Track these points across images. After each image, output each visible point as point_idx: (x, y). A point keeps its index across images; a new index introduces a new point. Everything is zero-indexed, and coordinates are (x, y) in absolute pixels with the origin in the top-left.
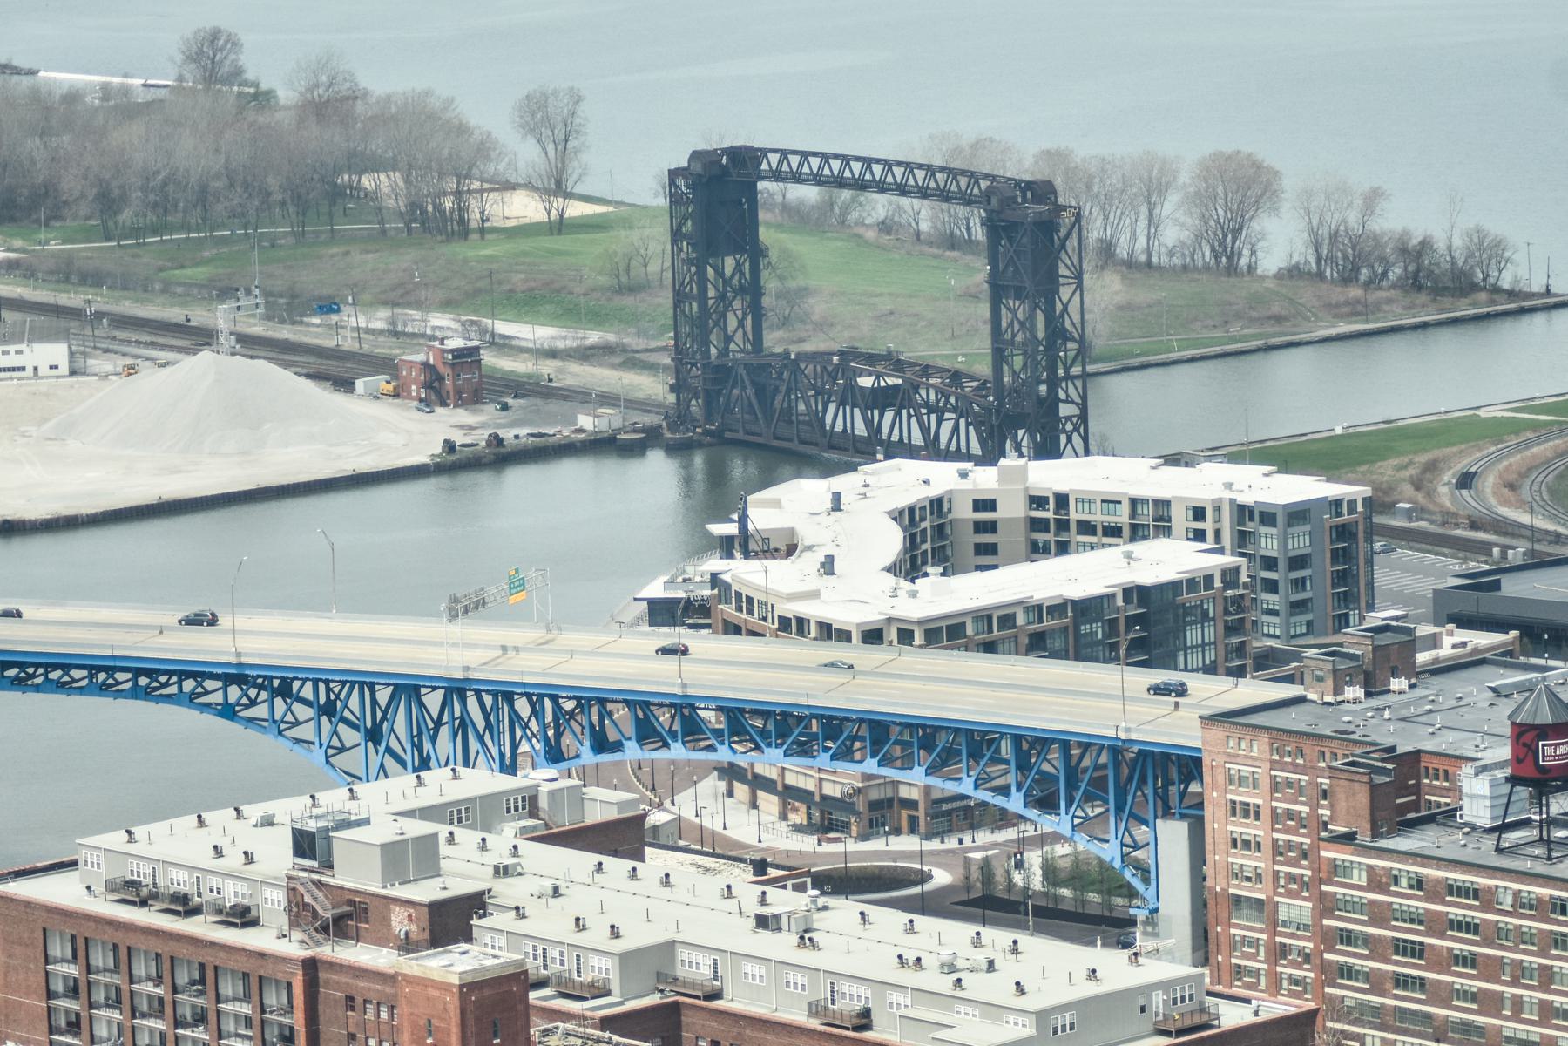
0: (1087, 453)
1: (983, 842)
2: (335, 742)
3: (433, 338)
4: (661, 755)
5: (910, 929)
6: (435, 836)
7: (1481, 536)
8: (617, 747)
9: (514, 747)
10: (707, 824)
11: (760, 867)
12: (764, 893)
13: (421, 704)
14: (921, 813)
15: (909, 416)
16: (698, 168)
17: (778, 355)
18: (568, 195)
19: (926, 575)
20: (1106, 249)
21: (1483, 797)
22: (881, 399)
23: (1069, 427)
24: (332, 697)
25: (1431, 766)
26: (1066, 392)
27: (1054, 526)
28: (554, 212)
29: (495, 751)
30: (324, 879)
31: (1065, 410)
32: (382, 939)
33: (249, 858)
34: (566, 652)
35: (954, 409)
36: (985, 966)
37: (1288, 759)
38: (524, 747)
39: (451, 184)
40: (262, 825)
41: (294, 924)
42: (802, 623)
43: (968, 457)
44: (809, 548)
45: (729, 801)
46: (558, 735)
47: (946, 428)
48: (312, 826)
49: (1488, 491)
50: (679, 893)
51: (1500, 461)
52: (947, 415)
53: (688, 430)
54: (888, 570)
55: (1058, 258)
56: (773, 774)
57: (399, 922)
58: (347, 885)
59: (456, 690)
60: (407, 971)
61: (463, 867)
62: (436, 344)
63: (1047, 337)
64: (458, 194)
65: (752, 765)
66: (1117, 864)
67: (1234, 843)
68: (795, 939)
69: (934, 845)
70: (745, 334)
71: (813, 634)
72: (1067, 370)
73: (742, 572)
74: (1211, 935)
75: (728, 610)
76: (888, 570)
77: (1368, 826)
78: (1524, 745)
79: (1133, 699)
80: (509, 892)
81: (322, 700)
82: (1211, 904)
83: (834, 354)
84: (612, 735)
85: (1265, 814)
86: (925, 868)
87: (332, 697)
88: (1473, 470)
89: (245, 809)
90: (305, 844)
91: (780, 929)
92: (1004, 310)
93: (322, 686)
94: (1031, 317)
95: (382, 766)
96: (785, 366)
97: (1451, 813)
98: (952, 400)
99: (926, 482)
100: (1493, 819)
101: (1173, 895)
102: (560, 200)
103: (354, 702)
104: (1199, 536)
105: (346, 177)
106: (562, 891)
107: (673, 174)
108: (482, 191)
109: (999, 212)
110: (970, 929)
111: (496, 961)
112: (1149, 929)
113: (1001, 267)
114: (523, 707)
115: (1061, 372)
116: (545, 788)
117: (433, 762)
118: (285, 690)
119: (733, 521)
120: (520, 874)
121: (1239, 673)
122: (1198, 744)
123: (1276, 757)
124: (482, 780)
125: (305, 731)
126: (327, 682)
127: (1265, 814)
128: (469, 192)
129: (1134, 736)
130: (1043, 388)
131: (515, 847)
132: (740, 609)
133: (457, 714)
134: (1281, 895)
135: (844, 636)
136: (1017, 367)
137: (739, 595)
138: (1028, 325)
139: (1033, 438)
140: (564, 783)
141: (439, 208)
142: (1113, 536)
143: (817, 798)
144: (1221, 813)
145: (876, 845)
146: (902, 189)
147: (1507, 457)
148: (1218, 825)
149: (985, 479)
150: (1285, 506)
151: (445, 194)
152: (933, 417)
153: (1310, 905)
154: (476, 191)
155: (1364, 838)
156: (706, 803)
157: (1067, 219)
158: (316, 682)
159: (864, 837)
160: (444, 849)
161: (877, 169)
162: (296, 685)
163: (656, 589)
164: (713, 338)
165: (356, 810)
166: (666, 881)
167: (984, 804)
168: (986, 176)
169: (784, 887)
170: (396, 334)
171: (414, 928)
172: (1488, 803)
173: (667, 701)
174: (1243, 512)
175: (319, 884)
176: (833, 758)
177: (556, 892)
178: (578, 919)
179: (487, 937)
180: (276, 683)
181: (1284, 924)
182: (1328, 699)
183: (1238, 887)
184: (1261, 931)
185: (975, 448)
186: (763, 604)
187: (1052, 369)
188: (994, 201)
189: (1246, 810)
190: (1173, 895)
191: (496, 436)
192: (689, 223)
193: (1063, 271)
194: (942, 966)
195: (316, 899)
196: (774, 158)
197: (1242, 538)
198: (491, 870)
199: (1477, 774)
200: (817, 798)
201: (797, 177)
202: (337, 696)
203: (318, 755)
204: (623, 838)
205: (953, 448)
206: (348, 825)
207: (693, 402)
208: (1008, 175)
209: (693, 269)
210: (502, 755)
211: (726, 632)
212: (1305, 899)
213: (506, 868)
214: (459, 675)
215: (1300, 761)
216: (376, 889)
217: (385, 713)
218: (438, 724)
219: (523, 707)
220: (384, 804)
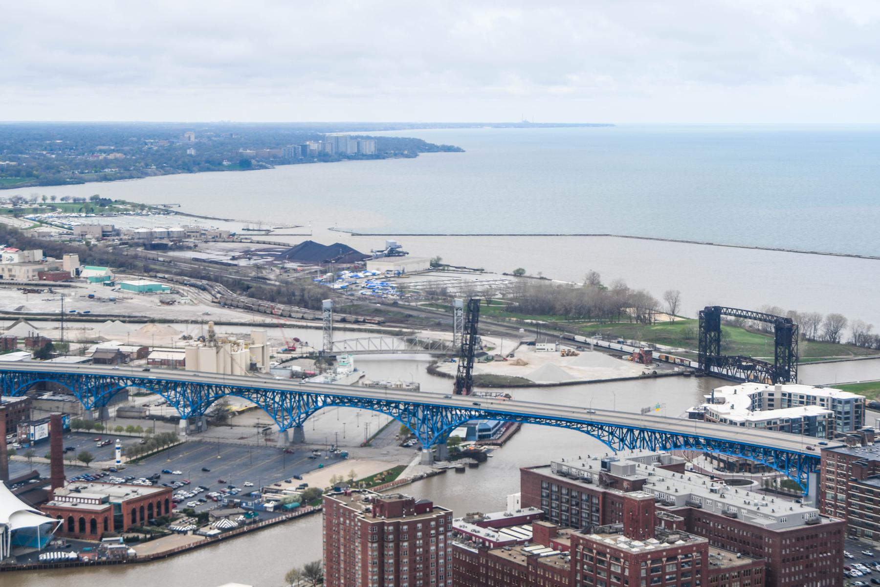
6: (634, 465)
11: (712, 478)
27: (788, 401)
31: (792, 373)
39: (648, 311)
42: (725, 420)
64: (649, 314)
73: (710, 406)
80: (653, 479)
104: (823, 405)
107: (701, 312)
135: (735, 424)
138: (784, 352)
145: (741, 474)
146: (755, 319)
156: (700, 461)
166: (689, 479)
174: (834, 400)
189: (830, 480)
197: (834, 407)
201: (730, 314)
204: (679, 468)
219: (658, 436)
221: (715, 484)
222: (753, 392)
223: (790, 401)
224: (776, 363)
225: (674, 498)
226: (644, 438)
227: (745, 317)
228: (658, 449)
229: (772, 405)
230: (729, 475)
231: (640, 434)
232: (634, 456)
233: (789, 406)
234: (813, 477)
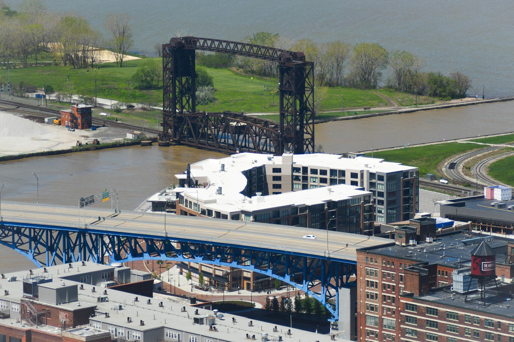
0: (314, 152)
1: (276, 293)
2: (37, 251)
3: (75, 104)
4: (158, 258)
5: (251, 324)
6: (76, 286)
7: (458, 186)
8: (141, 255)
9: (103, 255)
10: (173, 284)
11: (193, 300)
12: (197, 310)
13: (69, 238)
14: (251, 282)
15: (249, 137)
16: (173, 44)
17: (201, 113)
18: (124, 53)
19: (255, 195)
20: (322, 77)
21: (460, 282)
22: (239, 130)
23: (307, 142)
24: (36, 234)
25: (441, 270)
26: (307, 129)
27: (302, 178)
28: (119, 59)
29: (95, 256)
30: (34, 301)
31: (306, 136)
32: (55, 324)
33: (7, 293)
34: (123, 220)
35: (265, 135)
36: (278, 339)
37: (388, 266)
38: (107, 254)
39: (81, 47)
40: (12, 281)
41: (23, 318)
42: (210, 213)
43: (270, 153)
44: (213, 184)
45: (181, 276)
46: (119, 250)
47: (263, 141)
48: (31, 281)
49: (460, 170)
50: (166, 309)
51: (465, 159)
52: (263, 137)
53: (167, 140)
54: (242, 193)
55: (305, 81)
56: (197, 266)
57: (62, 318)
58: (43, 303)
59: (82, 232)
60: (66, 335)
61: (87, 297)
62: (75, 106)
63: (300, 110)
64: (84, 51)
65: (190, 263)
66: (324, 303)
67: (368, 296)
68: (209, 327)
69: (256, 294)
70: (189, 105)
71: (214, 216)
72: (307, 121)
73: (187, 192)
74: (358, 330)
75: (183, 206)
76: (242, 193)
77: (418, 291)
78: (476, 263)
79: (331, 243)
80: (102, 307)
81: (32, 235)
82: (358, 319)
83: (221, 114)
84: (139, 251)
85: (379, 286)
86: (253, 302)
87: (36, 234)
88: (455, 162)
89: (6, 275)
90: (30, 288)
91: (203, 324)
92: (285, 100)
93: (32, 230)
94: (295, 102)
95: (54, 260)
96: (204, 117)
97: (448, 287)
98: (265, 131)
99: (256, 161)
100: (464, 290)
101: (343, 316)
102: (121, 55)
103: (44, 237)
104: (354, 183)
105: (42, 44)
106: (123, 308)
107: (164, 46)
108: (93, 50)
109: (284, 64)
110: (273, 326)
111: (100, 333)
112: (335, 327)
113: (284, 83)
114: (107, 240)
115: (305, 122)
116: (117, 270)
117: (73, 259)
118: (18, 231)
119: (184, 173)
120: (108, 301)
121: (369, 234)
122: (355, 260)
123: (384, 265)
124: (92, 266)
125: (26, 247)
126: (34, 229)
127: (379, 286)
128: (88, 50)
129: (331, 256)
130: (298, 127)
131: (106, 291)
132: (186, 206)
133: (82, 241)
134: (384, 316)
135: (225, 217)
136: (289, 120)
137: (186, 200)
138: (294, 105)
139: (294, 146)
140: (125, 268)
141: (77, 56)
142: (323, 182)
143: (213, 276)
144: (364, 285)
145: (235, 293)
146: (248, 54)
147: (467, 158)
148: (362, 289)
149: (278, 161)
150: (387, 173)
151: (79, 51)
152: (258, 137)
153: (395, 320)
154: (90, 50)
155: (416, 296)
156: (173, 276)
157: (308, 67)
158: (30, 229)
159: (230, 290)
160: (79, 291)
161: (239, 46)
162: (23, 230)
163: (156, 198)
164: (177, 106)
165: (47, 276)
166: (161, 305)
167: (274, 279)
168: (280, 50)
169: (202, 308)
170: (60, 102)
171: (68, 320)
172: (462, 284)
173: (160, 239)
174: (372, 175)
175: (32, 303)
176: (220, 261)
177: (120, 308)
178: (128, 318)
179: (95, 324)
180: (15, 229)
181: (385, 326)
182: (404, 244)
183: (368, 312)
184: (377, 329)
185: (273, 150)
186: (195, 204)
187: (302, 121)
188: (282, 59)
189: (372, 284)
190: (343, 316)
191: (97, 140)
192: (170, 64)
193: (306, 85)
194: (263, 338)
195: (31, 308)
196: (202, 42)
197: (372, 185)
198: (97, 299)
199: (458, 274)
200: (213, 276)
201: (210, 49)
202: (38, 234)
203: (30, 255)
204: (146, 288)
205: (265, 149)
206: (43, 281)
207: (170, 130)
208: (287, 50)
209: (171, 81)
210: (98, 257)
211: (182, 214)
212: (393, 317)
213: (102, 298)
214: (83, 227)
215: (393, 267)
216: (54, 305)
217: (55, 240)
218: (75, 245)
219: (107, 240)
220: (58, 274)
221: (200, 310)
222: (249, 167)
223: (305, 179)
224: (282, 123)
225: (139, 334)
226: (85, 244)
227: (234, 52)
228: (106, 261)
229: (279, 186)
230: (216, 295)
231: (78, 237)
232: (73, 272)
233: (305, 187)
234: (345, 293)
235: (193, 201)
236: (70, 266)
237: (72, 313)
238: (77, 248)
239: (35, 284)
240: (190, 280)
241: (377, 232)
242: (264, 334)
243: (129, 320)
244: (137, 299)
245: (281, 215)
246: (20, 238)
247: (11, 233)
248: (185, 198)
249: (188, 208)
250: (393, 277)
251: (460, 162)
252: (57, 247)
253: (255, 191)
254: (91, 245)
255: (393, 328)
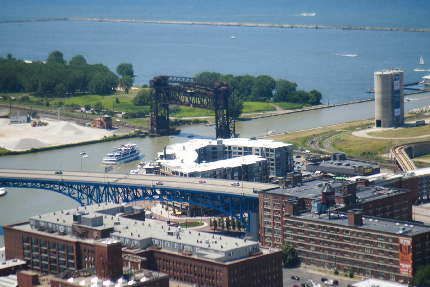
13: (99, 190)
32: (92, 237)
46: (127, 196)
48: (77, 214)
57: (95, 234)
59: (107, 186)
61: (109, 222)
68: (176, 237)
73: (164, 162)
79: (245, 188)
80: (117, 228)
84: (139, 196)
89: (64, 211)
114: (120, 190)
124: (112, 205)
132: (164, 170)
135: (185, 175)
137: (164, 167)
150: (276, 148)
156: (157, 208)
160: (104, 219)
166: (150, 225)
177: (127, 228)
189: (268, 210)
196: (171, 78)
201: (176, 82)
204: (141, 216)
210: (116, 200)
217: (92, 192)
218: (103, 194)
219: (120, 190)
220: (92, 211)
221: (171, 227)
223: (230, 153)
226: (109, 193)
231: (105, 189)
235: (168, 167)
236: (99, 206)
237: (100, 232)
238: (104, 195)
239: (80, 216)
240: (168, 211)
241: (270, 181)
242: (206, 240)
243: (132, 234)
244: (136, 223)
245: (217, 173)
246: (72, 191)
247: (67, 188)
248: (163, 166)
249: (165, 171)
250: (279, 206)
251: (317, 141)
252: (93, 195)
253: (202, 160)
254: (111, 193)
255: (280, 234)
